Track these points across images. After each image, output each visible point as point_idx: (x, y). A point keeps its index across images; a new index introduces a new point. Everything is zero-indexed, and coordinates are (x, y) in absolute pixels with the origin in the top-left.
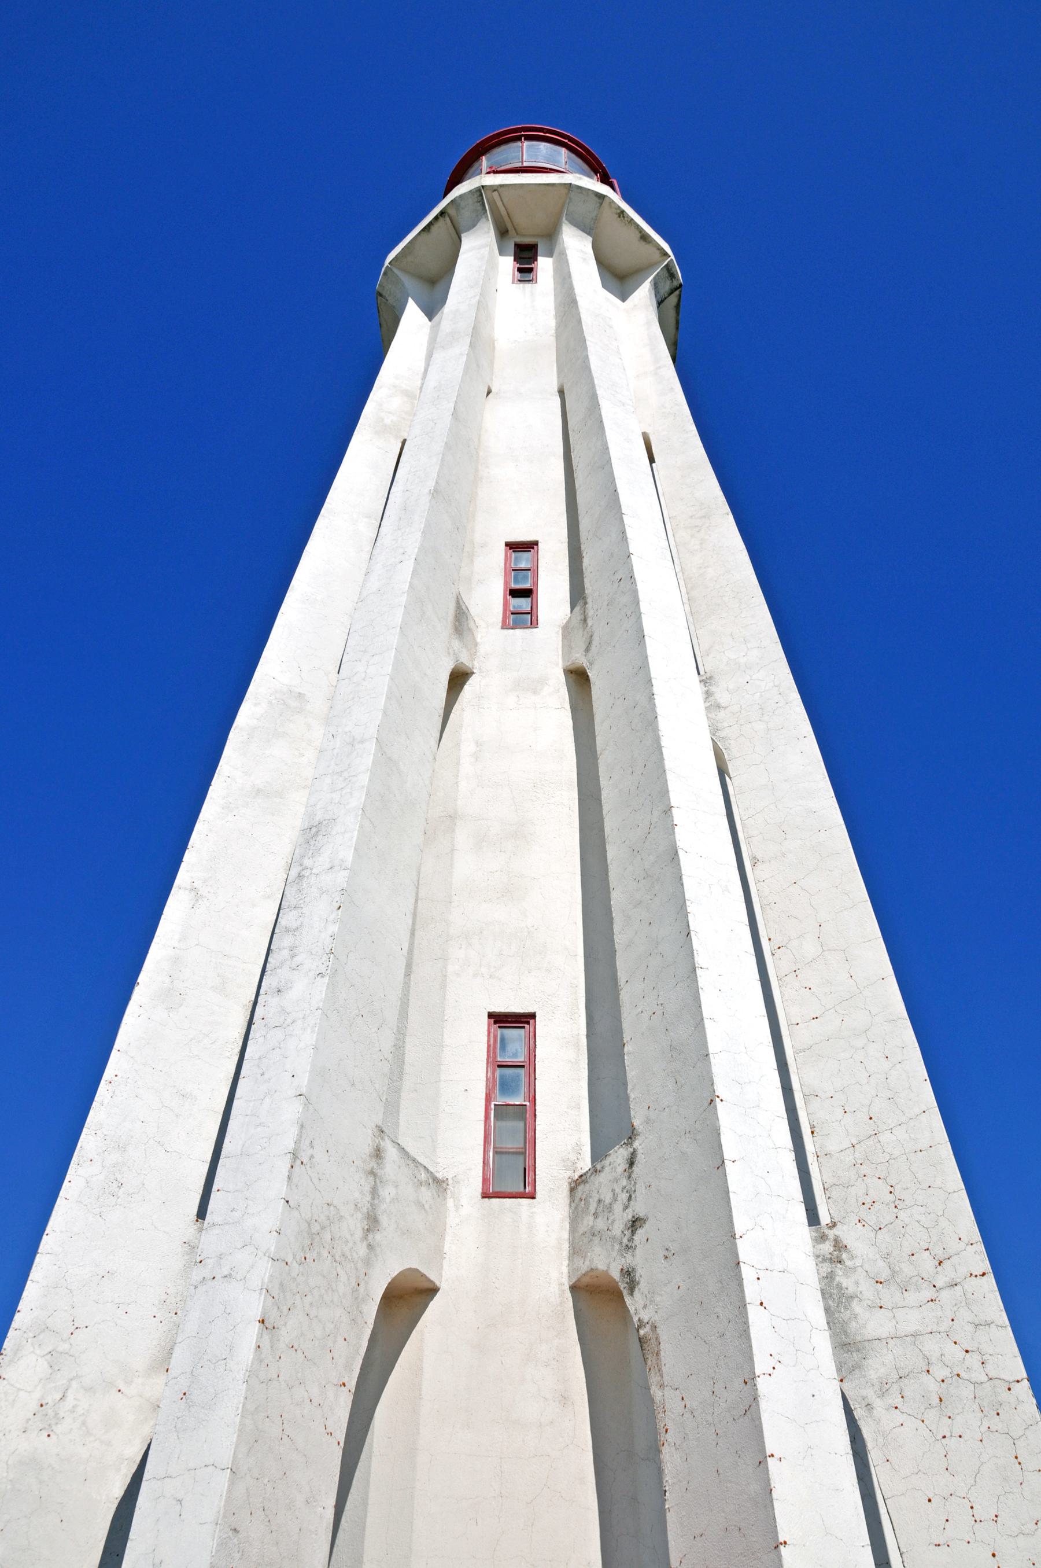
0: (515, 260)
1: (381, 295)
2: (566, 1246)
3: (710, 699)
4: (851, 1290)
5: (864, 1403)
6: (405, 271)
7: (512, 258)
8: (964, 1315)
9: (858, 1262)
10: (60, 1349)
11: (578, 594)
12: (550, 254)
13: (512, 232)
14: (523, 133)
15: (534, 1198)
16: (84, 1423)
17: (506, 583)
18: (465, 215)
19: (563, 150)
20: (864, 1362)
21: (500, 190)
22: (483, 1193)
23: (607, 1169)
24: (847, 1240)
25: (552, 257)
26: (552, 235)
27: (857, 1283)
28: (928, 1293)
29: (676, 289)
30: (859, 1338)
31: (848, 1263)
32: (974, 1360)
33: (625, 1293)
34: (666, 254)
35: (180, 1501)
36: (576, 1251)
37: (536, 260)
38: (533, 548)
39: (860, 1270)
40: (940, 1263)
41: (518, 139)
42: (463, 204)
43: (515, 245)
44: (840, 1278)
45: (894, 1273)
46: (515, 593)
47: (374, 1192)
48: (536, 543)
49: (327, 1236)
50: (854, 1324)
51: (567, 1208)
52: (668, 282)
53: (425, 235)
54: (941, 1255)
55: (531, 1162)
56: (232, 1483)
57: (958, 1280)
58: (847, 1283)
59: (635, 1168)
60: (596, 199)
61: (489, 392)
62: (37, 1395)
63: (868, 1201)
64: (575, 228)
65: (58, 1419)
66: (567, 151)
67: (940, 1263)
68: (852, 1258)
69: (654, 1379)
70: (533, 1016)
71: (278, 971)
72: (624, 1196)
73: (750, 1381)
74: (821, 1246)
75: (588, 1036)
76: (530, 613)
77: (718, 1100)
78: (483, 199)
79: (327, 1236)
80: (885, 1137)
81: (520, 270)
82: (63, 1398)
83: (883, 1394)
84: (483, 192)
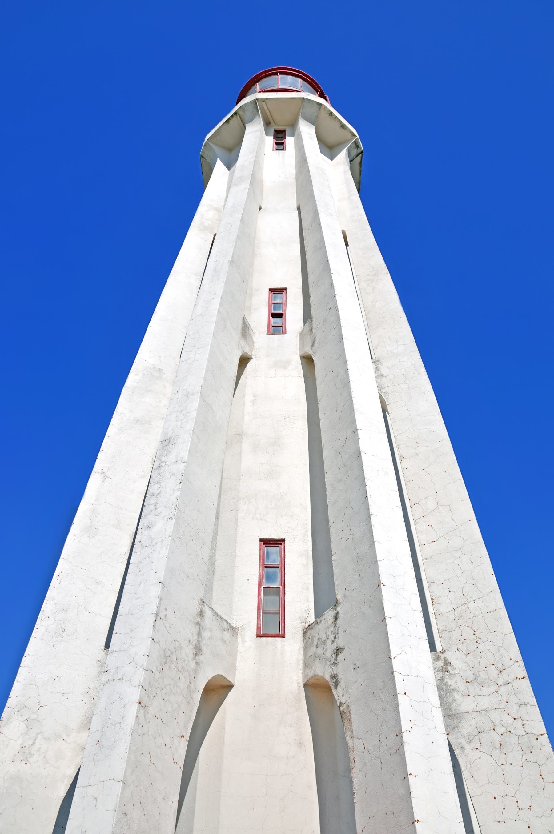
0: (274, 139)
1: (203, 157)
2: (301, 663)
3: (378, 372)
4: (453, 686)
9: (456, 671)
10: (32, 718)
11: (307, 316)
12: (293, 135)
14: (278, 71)
15: (284, 637)
17: (269, 310)
18: (247, 115)
21: (266, 101)
22: (257, 635)
23: (323, 622)
24: (451, 659)
25: (294, 137)
26: (294, 125)
28: (494, 688)
29: (360, 154)
31: (451, 672)
32: (518, 723)
33: (333, 688)
35: (96, 798)
36: (306, 665)
37: (286, 138)
39: (457, 675)
40: (500, 672)
41: (276, 74)
42: (246, 108)
44: (447, 680)
45: (476, 677)
46: (274, 315)
49: (174, 657)
50: (454, 704)
51: (302, 642)
54: (501, 668)
55: (283, 618)
56: (123, 789)
57: (510, 681)
58: (451, 682)
59: (338, 621)
63: (462, 639)
64: (306, 121)
67: (500, 672)
68: (454, 669)
69: (348, 733)
71: (148, 516)
73: (399, 734)
74: (437, 663)
77: (382, 585)
78: (257, 106)
79: (174, 657)
80: (471, 605)
81: (277, 144)
83: (470, 741)
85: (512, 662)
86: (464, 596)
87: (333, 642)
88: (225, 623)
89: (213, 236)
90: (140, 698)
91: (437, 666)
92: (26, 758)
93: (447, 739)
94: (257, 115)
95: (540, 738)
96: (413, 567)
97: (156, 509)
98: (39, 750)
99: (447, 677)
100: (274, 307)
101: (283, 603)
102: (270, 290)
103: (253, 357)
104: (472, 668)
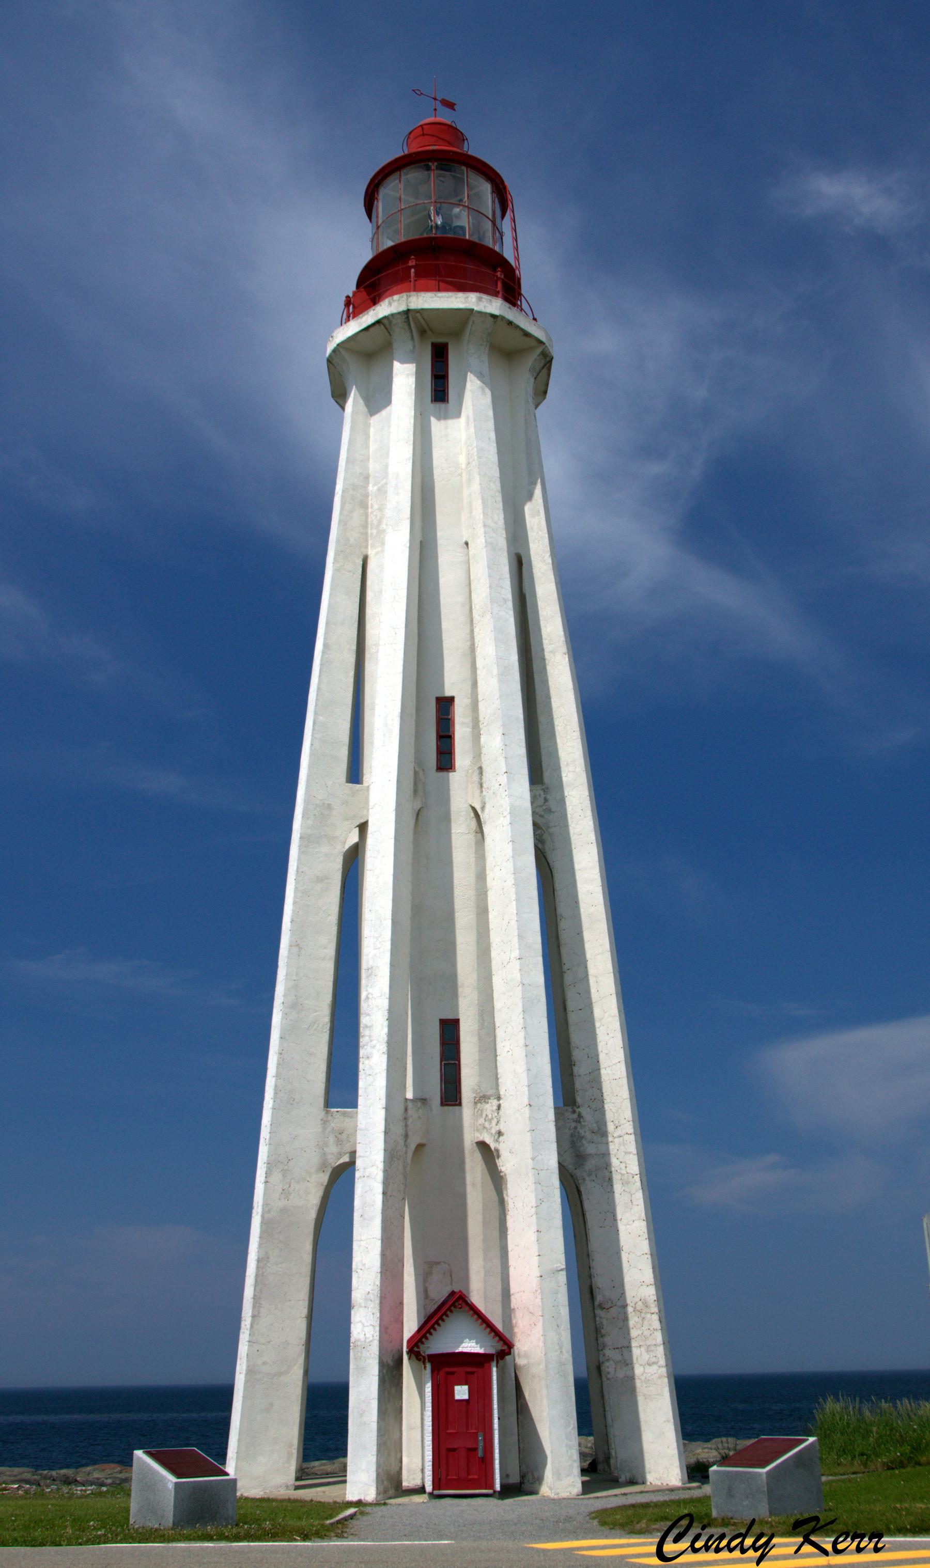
3: (547, 803)
4: (583, 1134)
8: (622, 1148)
9: (586, 1123)
16: (298, 1194)
23: (490, 1104)
27: (585, 1132)
31: (583, 1123)
32: (623, 1166)
33: (496, 1157)
35: (367, 1248)
42: (394, 321)
45: (599, 1129)
47: (406, 1125)
49: (395, 1153)
50: (582, 1148)
53: (365, 332)
54: (617, 1124)
58: (582, 1132)
60: (492, 319)
62: (281, 1186)
63: (593, 1098)
65: (290, 1194)
82: (290, 1186)
85: (625, 1121)
87: (497, 1125)
93: (468, 548)
95: (636, 1177)
98: (294, 1190)
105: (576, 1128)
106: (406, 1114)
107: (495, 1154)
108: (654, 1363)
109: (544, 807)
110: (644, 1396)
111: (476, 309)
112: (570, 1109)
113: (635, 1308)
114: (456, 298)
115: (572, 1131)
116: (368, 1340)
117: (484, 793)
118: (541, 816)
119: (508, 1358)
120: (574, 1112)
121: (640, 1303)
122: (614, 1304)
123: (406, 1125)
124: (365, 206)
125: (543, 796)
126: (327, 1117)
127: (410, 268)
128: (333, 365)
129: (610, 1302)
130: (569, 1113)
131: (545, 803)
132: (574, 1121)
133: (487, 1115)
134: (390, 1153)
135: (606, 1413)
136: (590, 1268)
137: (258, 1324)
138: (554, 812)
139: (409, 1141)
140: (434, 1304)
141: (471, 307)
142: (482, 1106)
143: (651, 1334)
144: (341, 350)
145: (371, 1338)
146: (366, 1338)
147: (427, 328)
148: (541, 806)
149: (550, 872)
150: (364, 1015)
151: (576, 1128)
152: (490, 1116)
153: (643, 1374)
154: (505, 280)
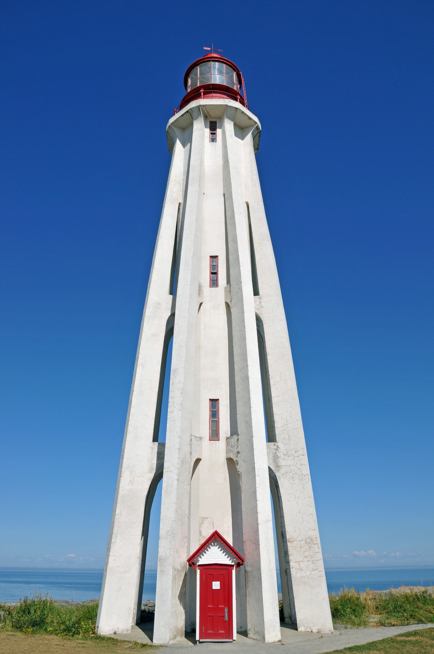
0: (210, 130)
1: (168, 133)
2: (225, 450)
3: (260, 304)
5: (279, 477)
6: (174, 126)
7: (209, 129)
9: (281, 450)
10: (132, 470)
11: (228, 282)
12: (220, 128)
13: (209, 117)
14: (211, 59)
15: (219, 440)
17: (210, 270)
18: (194, 115)
19: (224, 65)
20: (280, 470)
21: (205, 106)
22: (209, 440)
23: (233, 439)
24: (279, 446)
25: (221, 129)
26: (221, 118)
27: (280, 455)
28: (293, 458)
29: (259, 132)
30: (279, 465)
31: (279, 450)
32: (299, 471)
33: (236, 464)
34: (256, 123)
35: (168, 508)
36: (227, 452)
37: (216, 130)
38: (217, 257)
39: (281, 452)
40: (296, 452)
41: (210, 61)
42: (194, 110)
43: (210, 121)
44: (277, 453)
45: (287, 453)
46: (212, 273)
47: (191, 448)
48: (218, 256)
49: (185, 460)
50: (279, 463)
51: (226, 443)
52: (257, 131)
53: (182, 117)
54: (296, 450)
55: (218, 433)
56: (176, 505)
57: (299, 456)
59: (238, 441)
61: (204, 194)
63: (284, 438)
64: (228, 120)
66: (232, 551)
67: (296, 452)
68: (280, 449)
69: (241, 482)
70: (218, 399)
71: (171, 407)
72: (236, 446)
73: (255, 488)
74: (274, 447)
75: (230, 404)
76: (217, 280)
77: (253, 437)
78: (200, 109)
79: (185, 460)
80: (289, 425)
81: (212, 134)
82: (134, 479)
83: (283, 476)
84: (200, 107)
85: (300, 449)
86: (286, 421)
87: (237, 448)
88: (198, 438)
89: (178, 205)
90: (178, 478)
91: (274, 448)
92: (132, 484)
94: (200, 115)
96: (265, 427)
97: (174, 404)
99: (277, 452)
100: (212, 267)
101: (219, 431)
102: (210, 256)
103: (203, 302)
104: (286, 450)
105: (275, 453)
106: (191, 442)
107: (236, 463)
108: (316, 569)
109: (260, 306)
110: (311, 586)
111: (229, 105)
112: (272, 443)
113: (306, 541)
114: (220, 101)
115: (273, 455)
116: (167, 556)
117: (232, 294)
118: (258, 309)
119: (241, 567)
120: (275, 445)
121: (308, 539)
122: (295, 539)
123: (191, 448)
124: (184, 84)
125: (259, 300)
126: (154, 446)
127: (201, 92)
128: (169, 134)
129: (293, 538)
130: (273, 446)
131: (260, 303)
132: (275, 450)
133: (232, 444)
134: (182, 460)
135: (289, 594)
136: (282, 523)
137: (115, 547)
138: (264, 307)
139: (192, 455)
140: (204, 539)
141: (226, 104)
142: (229, 440)
143: (314, 555)
144: (173, 127)
145: (169, 555)
146: (166, 555)
147: (208, 115)
148: (258, 305)
149: (262, 339)
150: (171, 392)
151: (275, 453)
152: (233, 445)
153: (310, 575)
154: (241, 99)
